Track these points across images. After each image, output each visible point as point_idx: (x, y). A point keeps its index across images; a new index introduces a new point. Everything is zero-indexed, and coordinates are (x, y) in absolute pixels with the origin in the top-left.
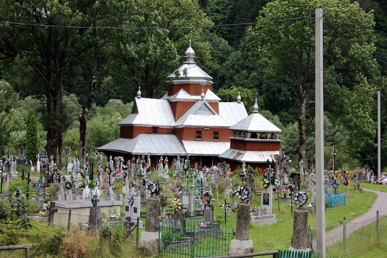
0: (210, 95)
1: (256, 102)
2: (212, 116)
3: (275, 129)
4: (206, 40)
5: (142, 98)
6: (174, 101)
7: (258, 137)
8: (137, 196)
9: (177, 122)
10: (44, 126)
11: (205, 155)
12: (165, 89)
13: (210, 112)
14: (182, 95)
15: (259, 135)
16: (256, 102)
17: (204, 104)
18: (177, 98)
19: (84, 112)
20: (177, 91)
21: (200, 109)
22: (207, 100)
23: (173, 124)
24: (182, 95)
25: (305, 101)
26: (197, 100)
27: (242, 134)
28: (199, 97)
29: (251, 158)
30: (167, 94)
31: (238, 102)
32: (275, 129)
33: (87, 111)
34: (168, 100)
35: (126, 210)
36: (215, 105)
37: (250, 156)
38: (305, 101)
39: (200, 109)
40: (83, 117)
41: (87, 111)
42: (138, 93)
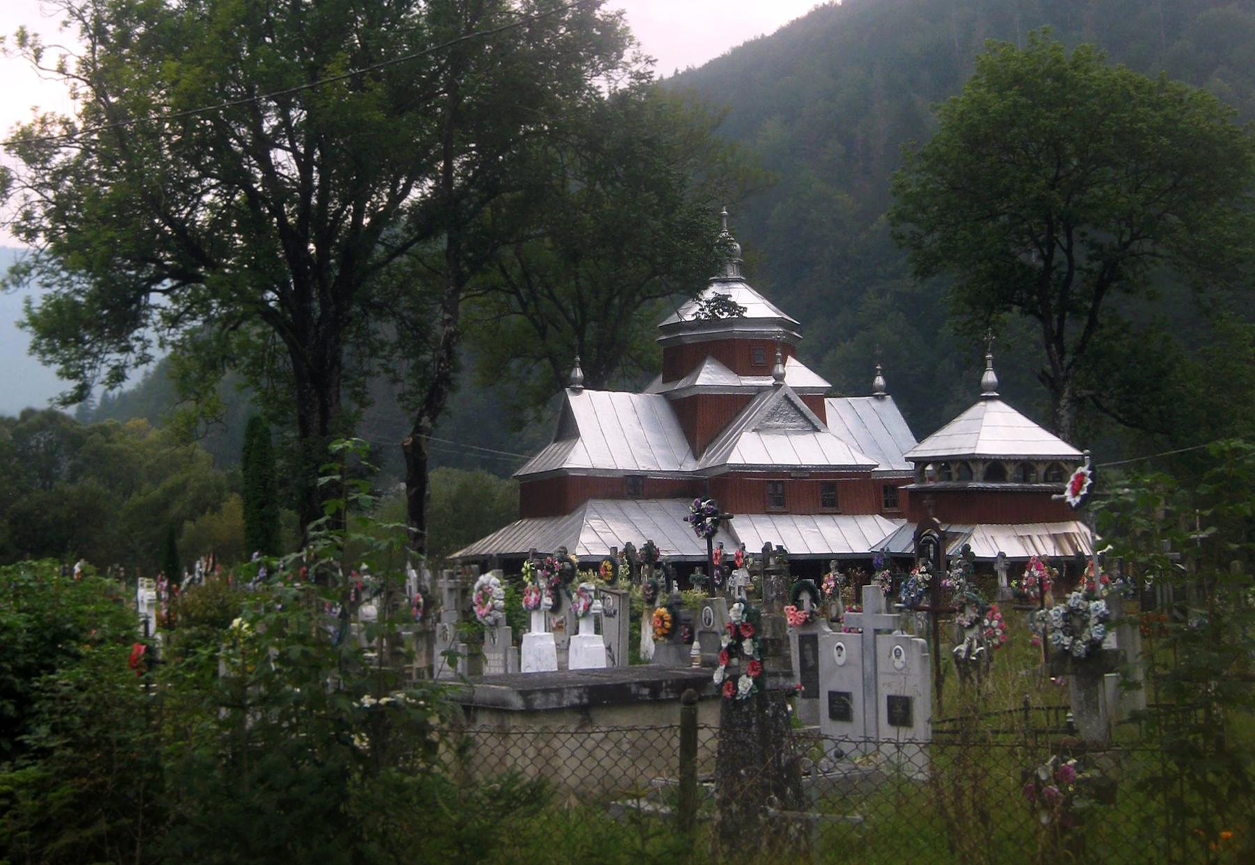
0: (798, 375)
1: (990, 364)
2: (810, 437)
3: (1050, 445)
4: (373, 505)
5: (586, 391)
6: (686, 394)
7: (1008, 477)
8: (877, 631)
9: (703, 459)
10: (623, 92)
11: (802, 558)
12: (99, 707)
13: (801, 422)
14: (711, 376)
15: (1010, 470)
16: (990, 364)
17: (786, 397)
18: (697, 383)
19: (418, 429)
20: (694, 367)
21: (772, 415)
22: (796, 389)
23: (690, 466)
24: (711, 376)
25: (1067, 390)
26: (761, 390)
27: (953, 469)
28: (770, 382)
29: (993, 545)
30: (660, 378)
31: (877, 397)
32: (1050, 445)
33: (429, 425)
34: (666, 395)
35: (893, 721)
36: (815, 400)
37: (990, 540)
38: (1067, 390)
39: (772, 415)
40: (416, 446)
41: (429, 425)
42: (573, 375)
